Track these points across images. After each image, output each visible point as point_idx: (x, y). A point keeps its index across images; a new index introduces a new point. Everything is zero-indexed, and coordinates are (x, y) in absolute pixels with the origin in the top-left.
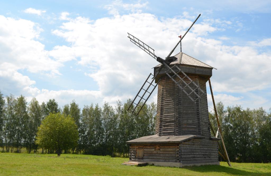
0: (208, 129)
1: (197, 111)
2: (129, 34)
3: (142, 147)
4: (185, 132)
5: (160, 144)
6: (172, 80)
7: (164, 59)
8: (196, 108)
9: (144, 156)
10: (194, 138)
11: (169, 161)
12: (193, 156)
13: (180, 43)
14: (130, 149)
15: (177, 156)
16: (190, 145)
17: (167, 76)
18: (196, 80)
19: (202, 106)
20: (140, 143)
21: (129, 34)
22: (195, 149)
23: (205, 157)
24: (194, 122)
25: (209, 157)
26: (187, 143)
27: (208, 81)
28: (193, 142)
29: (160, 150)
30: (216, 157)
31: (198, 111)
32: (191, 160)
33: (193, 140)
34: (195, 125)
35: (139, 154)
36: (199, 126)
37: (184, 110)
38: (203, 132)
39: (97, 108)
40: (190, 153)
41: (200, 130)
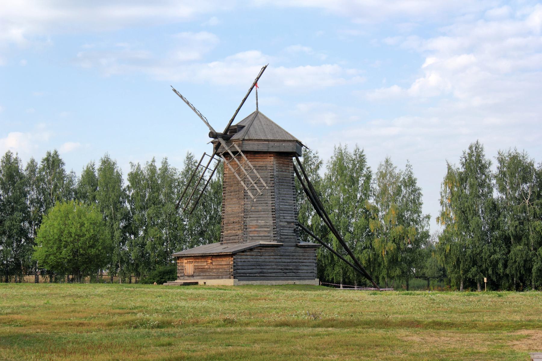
0: (293, 231)
1: (272, 206)
3: (192, 261)
4: (254, 238)
9: (194, 272)
11: (222, 278)
12: (261, 270)
15: (231, 271)
16: (253, 256)
17: (229, 154)
19: (281, 198)
20: (264, 245)
22: (270, 262)
23: (286, 273)
24: (267, 222)
26: (248, 253)
31: (273, 207)
32: (256, 276)
33: (260, 249)
34: (268, 228)
35: (189, 271)
37: (252, 206)
39: (165, 169)
40: (254, 267)
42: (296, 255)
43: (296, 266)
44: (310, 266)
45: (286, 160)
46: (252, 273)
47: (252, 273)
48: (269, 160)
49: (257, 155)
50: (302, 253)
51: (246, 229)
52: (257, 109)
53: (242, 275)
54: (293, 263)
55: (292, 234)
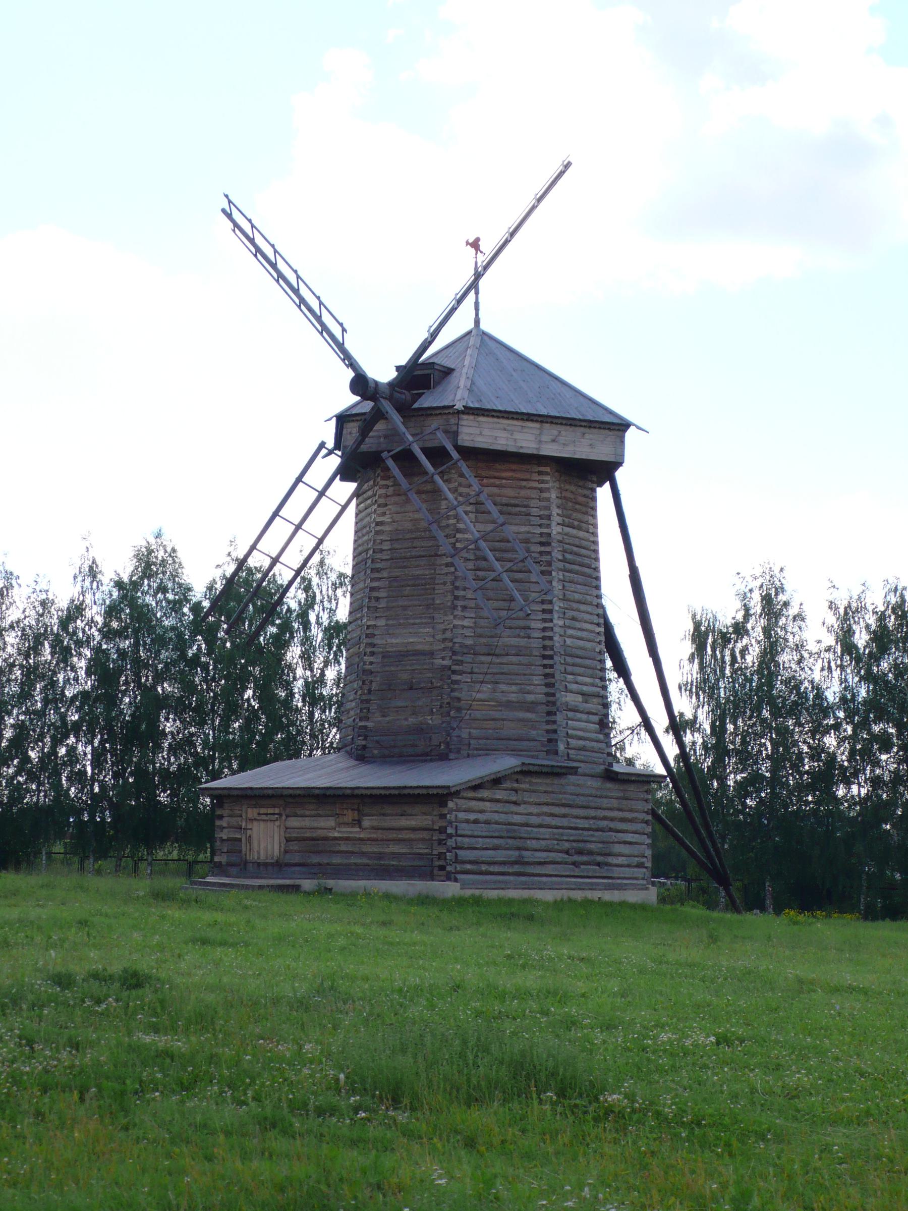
2: (230, 202)
3: (277, 811)
5: (362, 796)
6: (433, 482)
7: (397, 373)
8: (540, 625)
10: (522, 772)
12: (517, 853)
13: (472, 295)
14: (218, 823)
18: (547, 486)
19: (570, 614)
21: (230, 202)
25: (599, 864)
27: (607, 484)
28: (516, 791)
29: (360, 827)
30: (640, 865)
33: (517, 781)
36: (549, 713)
38: (568, 743)
41: (555, 731)
42: (604, 806)
43: (603, 842)
44: (636, 843)
45: (580, 491)
46: (495, 863)
47: (495, 863)
48: (536, 485)
49: (498, 466)
50: (618, 798)
51: (459, 710)
52: (477, 322)
53: (469, 867)
54: (597, 834)
55: (593, 736)
